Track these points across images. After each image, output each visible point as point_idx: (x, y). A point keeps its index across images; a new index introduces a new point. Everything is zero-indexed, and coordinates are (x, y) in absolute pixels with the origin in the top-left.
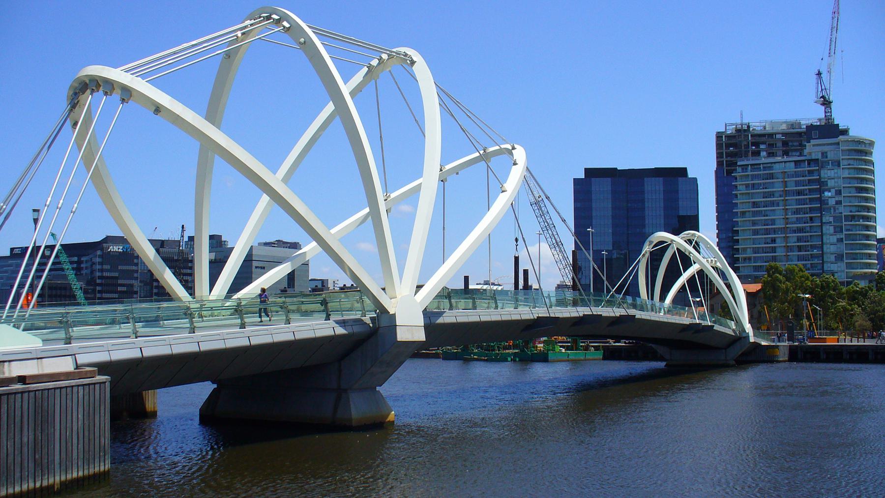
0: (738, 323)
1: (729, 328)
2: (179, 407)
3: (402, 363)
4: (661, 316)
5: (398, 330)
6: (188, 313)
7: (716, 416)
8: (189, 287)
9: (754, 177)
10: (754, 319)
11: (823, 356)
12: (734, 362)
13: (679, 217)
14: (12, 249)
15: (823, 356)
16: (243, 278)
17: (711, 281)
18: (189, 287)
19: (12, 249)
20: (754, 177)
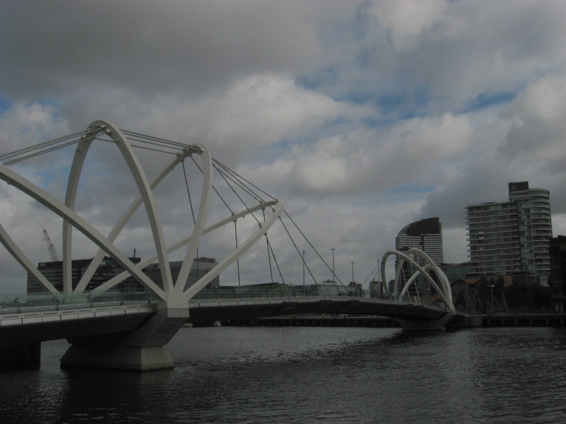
0: (447, 306)
1: (440, 308)
2: (53, 352)
3: (176, 331)
4: (400, 302)
5: (169, 312)
6: (55, 301)
7: (459, 352)
8: (60, 287)
9: (478, 214)
10: (455, 304)
11: (503, 323)
12: (444, 328)
13: (553, 240)
14: (39, 264)
15: (503, 323)
16: (94, 284)
17: (201, 291)
18: (60, 287)
19: (39, 264)
20: (478, 214)
